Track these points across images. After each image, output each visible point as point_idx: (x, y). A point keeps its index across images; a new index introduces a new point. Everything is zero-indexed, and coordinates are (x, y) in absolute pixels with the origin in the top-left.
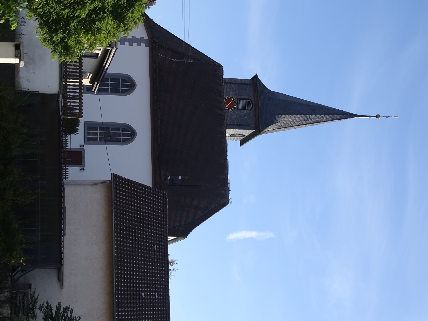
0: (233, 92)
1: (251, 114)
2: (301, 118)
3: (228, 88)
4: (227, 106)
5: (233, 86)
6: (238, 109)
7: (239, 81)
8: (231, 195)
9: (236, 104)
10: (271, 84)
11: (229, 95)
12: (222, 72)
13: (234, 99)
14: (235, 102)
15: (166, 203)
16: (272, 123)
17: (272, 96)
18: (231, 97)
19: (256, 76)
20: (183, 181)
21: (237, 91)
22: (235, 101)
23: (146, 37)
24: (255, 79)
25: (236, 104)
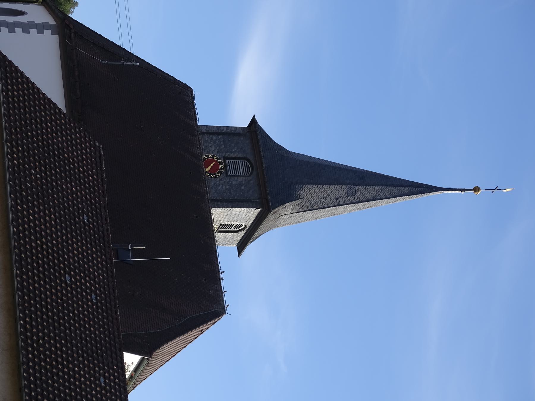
0: (215, 148)
1: (251, 182)
2: (342, 190)
3: (207, 141)
4: (207, 170)
5: (214, 137)
6: (227, 175)
7: (225, 129)
8: (228, 299)
9: (222, 166)
10: (283, 134)
11: (211, 153)
12: (195, 111)
13: (218, 159)
14: (221, 164)
15: (101, 162)
16: (291, 198)
17: (285, 155)
18: (213, 156)
19: (254, 121)
20: (136, 253)
21: (223, 146)
22: (220, 161)
23: (51, 21)
24: (253, 125)
25: (222, 166)
